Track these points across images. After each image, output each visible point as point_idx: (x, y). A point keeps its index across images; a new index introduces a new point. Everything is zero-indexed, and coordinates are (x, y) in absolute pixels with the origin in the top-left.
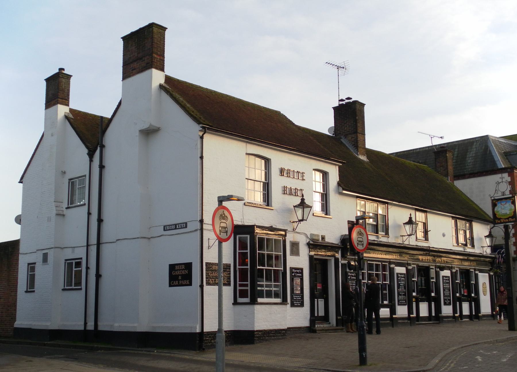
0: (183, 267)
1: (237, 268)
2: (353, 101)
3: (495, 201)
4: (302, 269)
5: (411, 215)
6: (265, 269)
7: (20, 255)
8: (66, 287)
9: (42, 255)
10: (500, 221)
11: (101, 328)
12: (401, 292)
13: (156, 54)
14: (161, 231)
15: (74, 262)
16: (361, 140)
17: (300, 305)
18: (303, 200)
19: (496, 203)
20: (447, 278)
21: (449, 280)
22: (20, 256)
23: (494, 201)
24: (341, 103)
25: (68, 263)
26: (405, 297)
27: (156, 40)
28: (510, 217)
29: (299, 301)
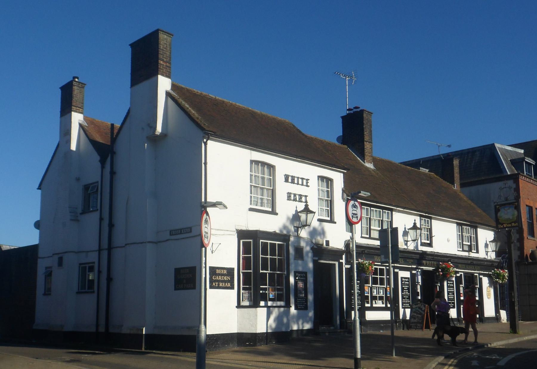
0: (225, 272)
1: (241, 272)
2: (360, 110)
3: (499, 206)
4: (234, 268)
5: (415, 221)
6: (268, 273)
8: (80, 291)
10: (503, 226)
11: (111, 330)
12: (404, 296)
13: (161, 61)
16: (368, 148)
17: (303, 308)
18: (307, 206)
19: (499, 208)
20: (451, 282)
21: (453, 284)
22: (39, 261)
26: (408, 301)
27: (162, 46)
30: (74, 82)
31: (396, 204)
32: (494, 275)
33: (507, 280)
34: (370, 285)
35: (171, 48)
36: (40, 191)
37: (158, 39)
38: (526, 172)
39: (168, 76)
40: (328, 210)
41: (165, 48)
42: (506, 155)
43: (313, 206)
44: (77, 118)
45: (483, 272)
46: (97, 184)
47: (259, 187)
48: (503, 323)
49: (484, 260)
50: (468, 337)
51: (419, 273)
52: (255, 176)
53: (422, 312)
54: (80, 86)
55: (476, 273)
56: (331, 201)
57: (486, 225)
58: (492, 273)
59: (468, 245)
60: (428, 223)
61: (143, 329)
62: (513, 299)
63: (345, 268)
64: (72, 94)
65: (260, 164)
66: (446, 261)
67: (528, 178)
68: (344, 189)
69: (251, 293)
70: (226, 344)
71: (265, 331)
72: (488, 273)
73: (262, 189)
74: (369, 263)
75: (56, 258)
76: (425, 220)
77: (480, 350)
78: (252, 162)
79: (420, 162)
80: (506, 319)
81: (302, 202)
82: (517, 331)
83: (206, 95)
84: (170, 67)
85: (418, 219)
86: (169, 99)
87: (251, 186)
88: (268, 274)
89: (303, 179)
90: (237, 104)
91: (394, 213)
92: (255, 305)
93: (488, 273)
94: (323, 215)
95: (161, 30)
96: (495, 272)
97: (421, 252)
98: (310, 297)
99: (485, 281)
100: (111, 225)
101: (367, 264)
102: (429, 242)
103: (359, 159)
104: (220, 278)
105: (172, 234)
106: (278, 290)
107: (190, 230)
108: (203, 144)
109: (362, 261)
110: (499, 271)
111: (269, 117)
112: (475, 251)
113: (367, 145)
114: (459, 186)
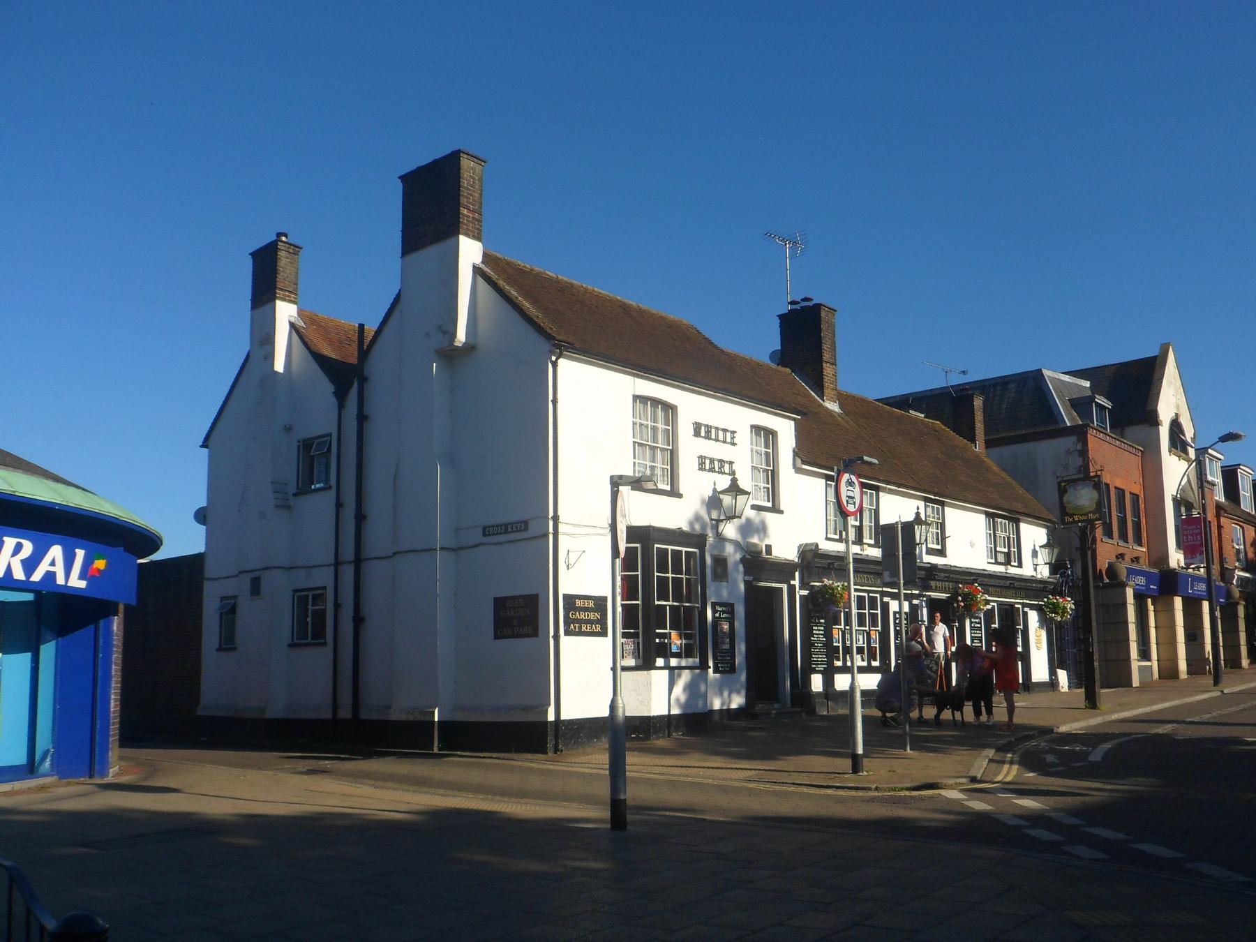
0: (591, 604)
5: (918, 508)
6: (669, 605)
7: (205, 582)
8: (295, 641)
9: (249, 582)
11: (365, 715)
14: (477, 536)
15: (310, 594)
16: (829, 374)
18: (734, 481)
20: (977, 620)
21: (980, 623)
22: (207, 586)
23: (1063, 484)
24: (794, 307)
25: (298, 597)
28: (1090, 512)
29: (727, 663)
30: (279, 243)
31: (886, 479)
32: (1048, 607)
33: (1070, 615)
34: (842, 627)
35: (481, 186)
36: (205, 451)
37: (459, 169)
38: (1097, 421)
39: (477, 237)
40: (769, 488)
41: (472, 186)
42: (1063, 391)
43: (745, 483)
44: (285, 312)
45: (1030, 601)
46: (329, 438)
47: (647, 445)
48: (1062, 692)
49: (1032, 580)
50: (1014, 717)
51: (924, 603)
52: (641, 425)
53: (933, 674)
54: (291, 251)
55: (1018, 602)
56: (773, 471)
57: (1036, 518)
58: (1043, 603)
59: (1004, 553)
60: (938, 514)
61: (434, 712)
62: (1091, 649)
63: (800, 595)
64: (276, 266)
65: (649, 402)
66: (969, 581)
67: (1102, 432)
68: (796, 450)
69: (638, 643)
70: (595, 737)
71: (666, 713)
72: (1037, 603)
73: (653, 449)
74: (843, 585)
75: (246, 581)
76: (933, 507)
77: (1048, 737)
78: (635, 397)
79: (908, 399)
80: (1067, 684)
81: (724, 473)
82: (1098, 705)
83: (540, 273)
84: (481, 221)
85: (921, 504)
86: (480, 280)
87: (634, 442)
88: (668, 607)
89: (725, 431)
90: (596, 289)
91: (881, 494)
92: (646, 664)
93: (1037, 603)
94: (760, 498)
95: (464, 153)
96: (1050, 601)
97: (929, 565)
98: (741, 648)
99: (1033, 616)
100: (360, 517)
101: (839, 589)
102: (939, 547)
103: (813, 394)
104: (581, 616)
105: (487, 533)
106: (687, 637)
107: (524, 525)
108: (550, 366)
109: (831, 582)
110: (1057, 599)
111: (653, 314)
112: (1016, 564)
113: (828, 369)
114: (983, 446)
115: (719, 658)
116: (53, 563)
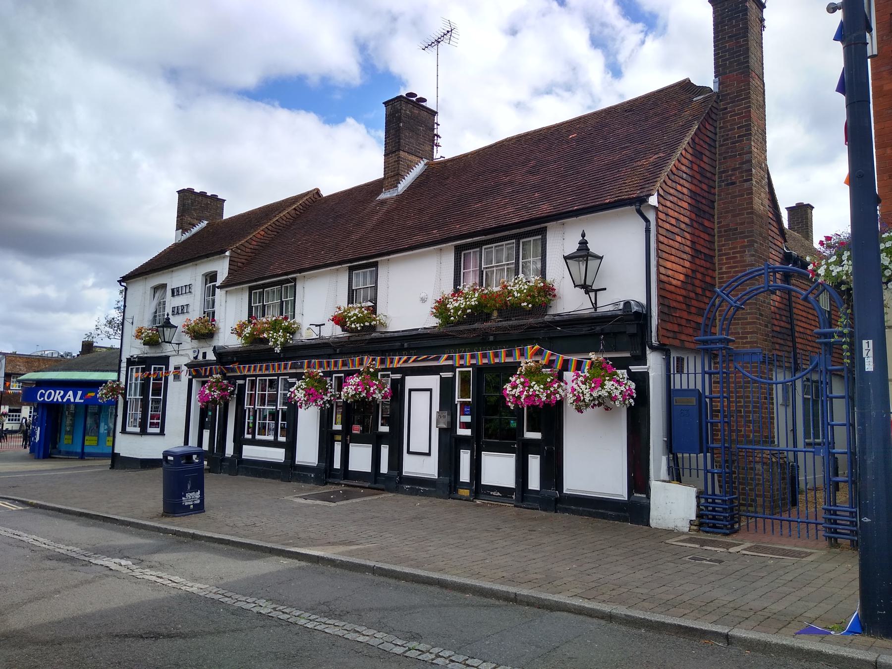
115: (849, 523)
116: (69, 396)
